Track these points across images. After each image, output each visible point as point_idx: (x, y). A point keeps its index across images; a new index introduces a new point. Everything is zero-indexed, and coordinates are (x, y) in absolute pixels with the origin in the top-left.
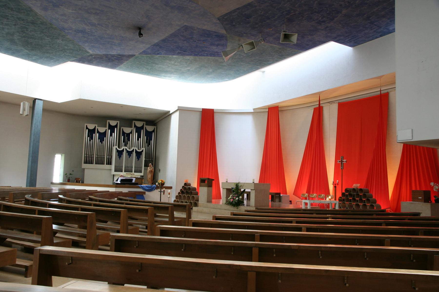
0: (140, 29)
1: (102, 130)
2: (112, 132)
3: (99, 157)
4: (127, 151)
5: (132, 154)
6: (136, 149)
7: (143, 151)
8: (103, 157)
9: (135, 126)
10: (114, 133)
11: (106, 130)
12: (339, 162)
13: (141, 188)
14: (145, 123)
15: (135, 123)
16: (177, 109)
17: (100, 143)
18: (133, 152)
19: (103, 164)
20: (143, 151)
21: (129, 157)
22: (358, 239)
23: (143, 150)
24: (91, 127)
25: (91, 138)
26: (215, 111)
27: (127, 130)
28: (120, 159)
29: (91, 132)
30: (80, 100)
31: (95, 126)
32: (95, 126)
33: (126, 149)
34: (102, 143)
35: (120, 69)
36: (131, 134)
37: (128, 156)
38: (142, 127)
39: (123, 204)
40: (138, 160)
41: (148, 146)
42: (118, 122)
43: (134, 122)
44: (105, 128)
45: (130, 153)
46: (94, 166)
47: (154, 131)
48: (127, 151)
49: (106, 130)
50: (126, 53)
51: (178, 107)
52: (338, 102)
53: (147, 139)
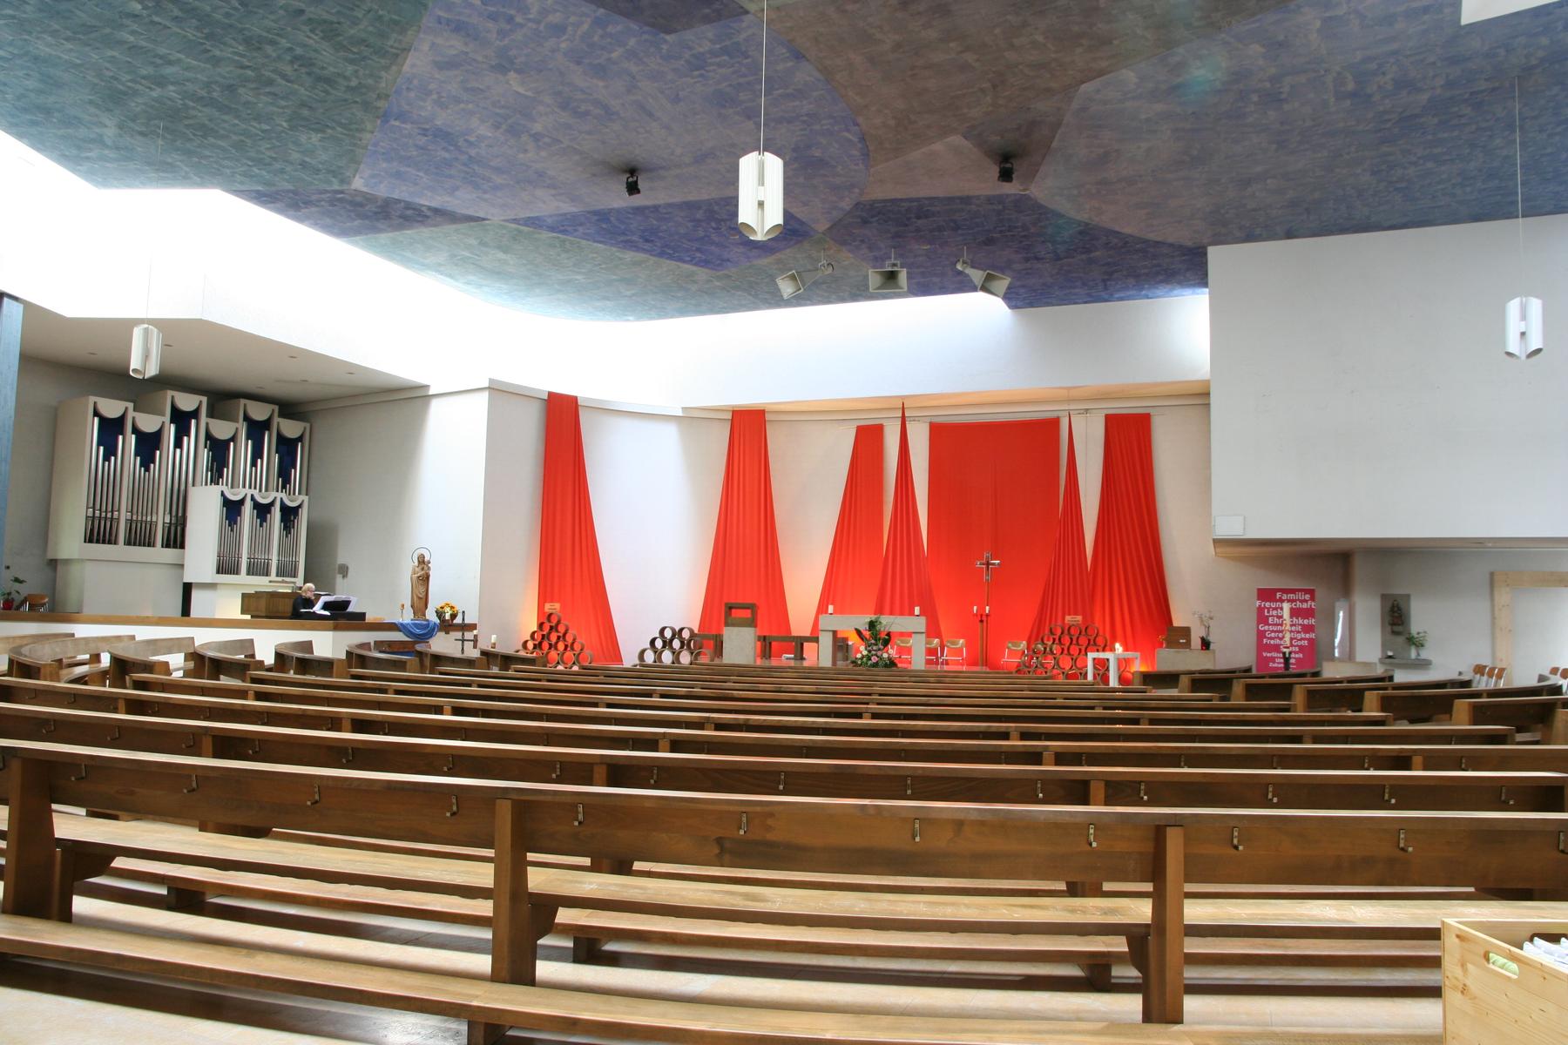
0: (632, 171)
1: (149, 423)
2: (182, 432)
3: (100, 517)
5: (269, 516)
6: (281, 499)
8: (112, 518)
9: (247, 418)
10: (189, 436)
13: (401, 631)
14: (276, 408)
15: (245, 405)
17: (143, 469)
18: (273, 508)
19: (151, 544)
21: (261, 525)
23: (303, 501)
24: (112, 408)
25: (110, 451)
27: (222, 430)
28: (232, 530)
29: (111, 429)
30: (200, 321)
32: (126, 408)
33: (252, 496)
34: (147, 470)
35: (356, 244)
36: (232, 444)
37: (259, 520)
38: (266, 425)
40: (287, 536)
41: (107, 458)
43: (243, 401)
44: (163, 419)
46: (120, 550)
47: (300, 439)
50: (428, 200)
51: (491, 380)
52: (929, 420)
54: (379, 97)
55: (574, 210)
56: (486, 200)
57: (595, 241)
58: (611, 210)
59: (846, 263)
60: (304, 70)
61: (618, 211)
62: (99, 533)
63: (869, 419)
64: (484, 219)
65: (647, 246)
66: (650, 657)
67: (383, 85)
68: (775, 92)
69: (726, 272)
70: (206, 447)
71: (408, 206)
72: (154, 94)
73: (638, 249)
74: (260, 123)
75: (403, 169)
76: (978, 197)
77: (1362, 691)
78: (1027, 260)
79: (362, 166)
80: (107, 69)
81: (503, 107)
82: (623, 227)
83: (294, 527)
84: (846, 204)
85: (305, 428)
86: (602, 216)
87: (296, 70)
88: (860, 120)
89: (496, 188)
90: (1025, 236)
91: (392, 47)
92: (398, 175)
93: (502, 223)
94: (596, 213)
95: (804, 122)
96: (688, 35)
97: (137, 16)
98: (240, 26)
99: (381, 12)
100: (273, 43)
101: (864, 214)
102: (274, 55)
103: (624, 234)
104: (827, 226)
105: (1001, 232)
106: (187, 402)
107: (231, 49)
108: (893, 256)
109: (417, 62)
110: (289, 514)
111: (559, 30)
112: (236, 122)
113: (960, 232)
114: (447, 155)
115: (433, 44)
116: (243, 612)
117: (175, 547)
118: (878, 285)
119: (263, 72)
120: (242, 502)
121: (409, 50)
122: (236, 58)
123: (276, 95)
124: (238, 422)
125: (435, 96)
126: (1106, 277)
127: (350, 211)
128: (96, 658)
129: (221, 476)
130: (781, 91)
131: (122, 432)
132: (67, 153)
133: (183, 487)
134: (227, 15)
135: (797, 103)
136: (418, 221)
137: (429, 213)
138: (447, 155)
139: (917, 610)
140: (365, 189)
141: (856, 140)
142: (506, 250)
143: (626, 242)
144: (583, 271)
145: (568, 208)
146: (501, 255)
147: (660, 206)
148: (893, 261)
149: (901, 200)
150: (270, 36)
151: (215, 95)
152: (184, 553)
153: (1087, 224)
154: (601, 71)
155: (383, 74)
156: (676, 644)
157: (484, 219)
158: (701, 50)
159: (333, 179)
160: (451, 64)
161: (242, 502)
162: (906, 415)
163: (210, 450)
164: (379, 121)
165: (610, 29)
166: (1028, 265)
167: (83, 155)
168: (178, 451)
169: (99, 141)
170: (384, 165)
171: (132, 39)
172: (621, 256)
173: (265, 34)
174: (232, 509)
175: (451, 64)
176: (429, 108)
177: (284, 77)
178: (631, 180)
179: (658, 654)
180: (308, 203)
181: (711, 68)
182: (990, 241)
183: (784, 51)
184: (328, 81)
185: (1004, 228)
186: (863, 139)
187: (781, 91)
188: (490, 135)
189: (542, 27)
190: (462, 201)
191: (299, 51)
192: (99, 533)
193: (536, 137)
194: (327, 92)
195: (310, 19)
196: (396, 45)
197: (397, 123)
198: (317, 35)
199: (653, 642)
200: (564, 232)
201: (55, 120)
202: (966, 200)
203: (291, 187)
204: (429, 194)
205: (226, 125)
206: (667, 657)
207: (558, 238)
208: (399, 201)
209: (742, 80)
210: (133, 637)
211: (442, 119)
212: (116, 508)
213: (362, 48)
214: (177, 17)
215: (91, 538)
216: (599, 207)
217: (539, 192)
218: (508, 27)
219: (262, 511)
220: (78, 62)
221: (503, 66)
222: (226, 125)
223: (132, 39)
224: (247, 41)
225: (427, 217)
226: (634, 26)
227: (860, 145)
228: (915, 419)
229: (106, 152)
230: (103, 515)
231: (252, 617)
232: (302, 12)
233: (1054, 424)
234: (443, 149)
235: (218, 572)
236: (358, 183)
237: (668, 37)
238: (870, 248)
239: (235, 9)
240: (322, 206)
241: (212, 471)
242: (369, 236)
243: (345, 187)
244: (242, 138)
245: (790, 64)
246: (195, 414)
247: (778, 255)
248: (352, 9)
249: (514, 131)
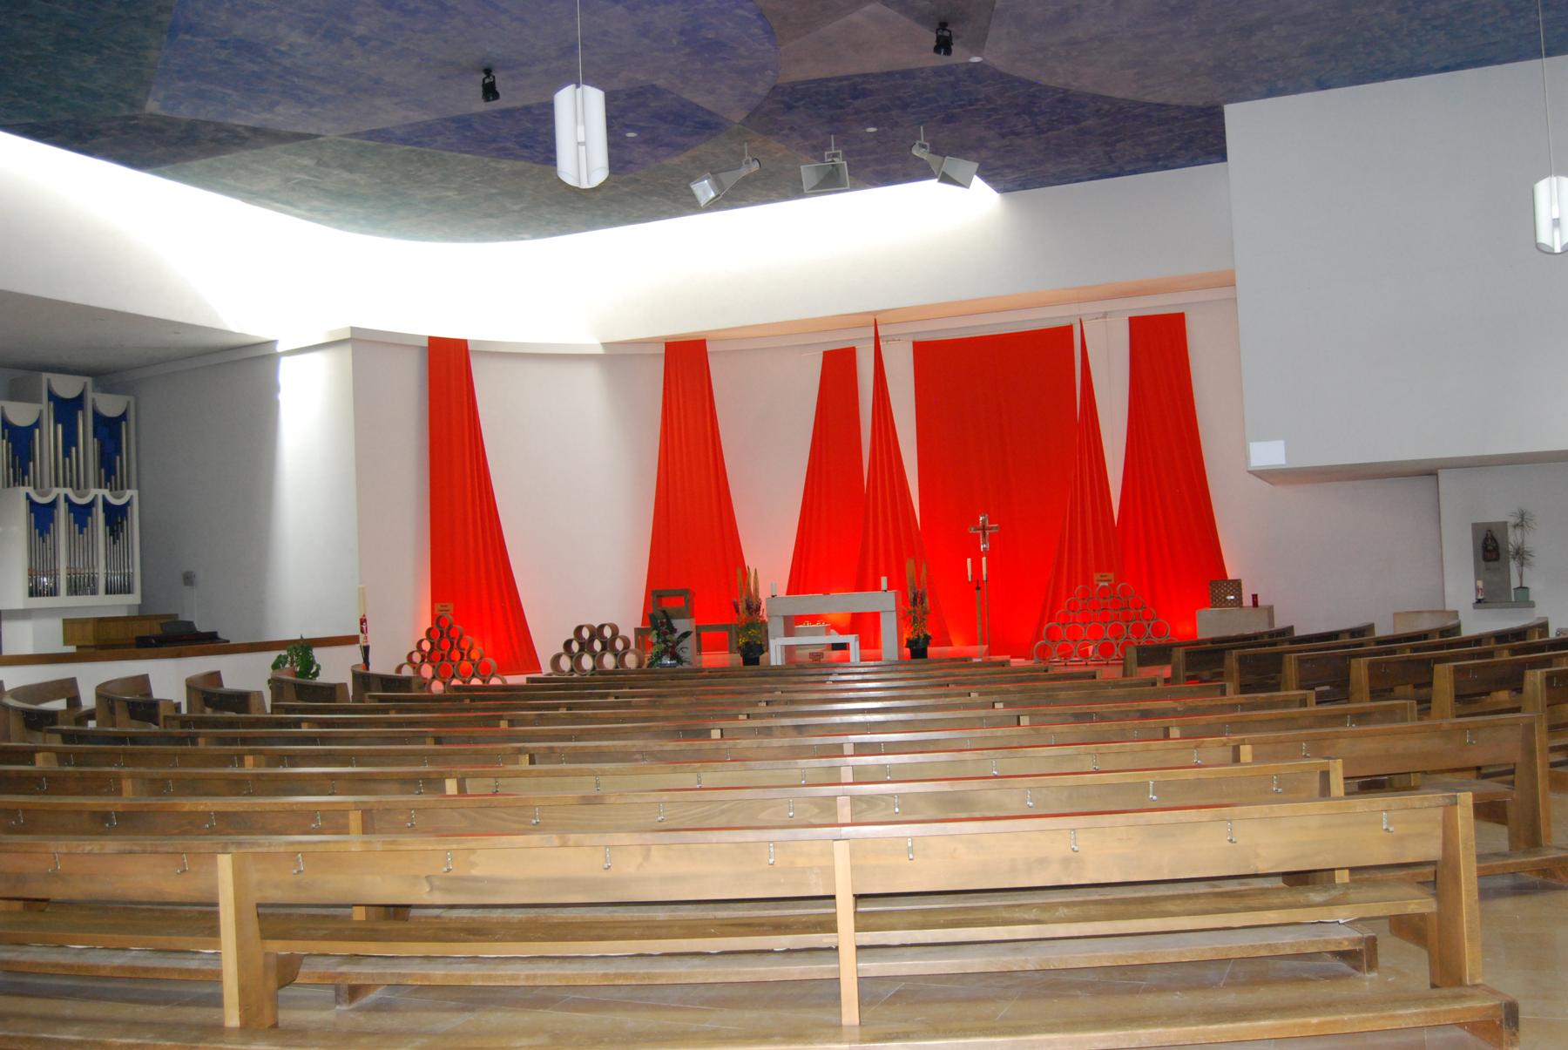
4: (72, 506)
9: (52, 396)
12: (990, 528)
21: (81, 532)
37: (77, 526)
38: (78, 402)
39: (572, 689)
40: (114, 543)
43: (45, 376)
45: (81, 514)
47: (124, 416)
48: (72, 506)
53: (102, 446)
63: (838, 341)
116: (66, 642)
139: (884, 580)
231: (78, 647)
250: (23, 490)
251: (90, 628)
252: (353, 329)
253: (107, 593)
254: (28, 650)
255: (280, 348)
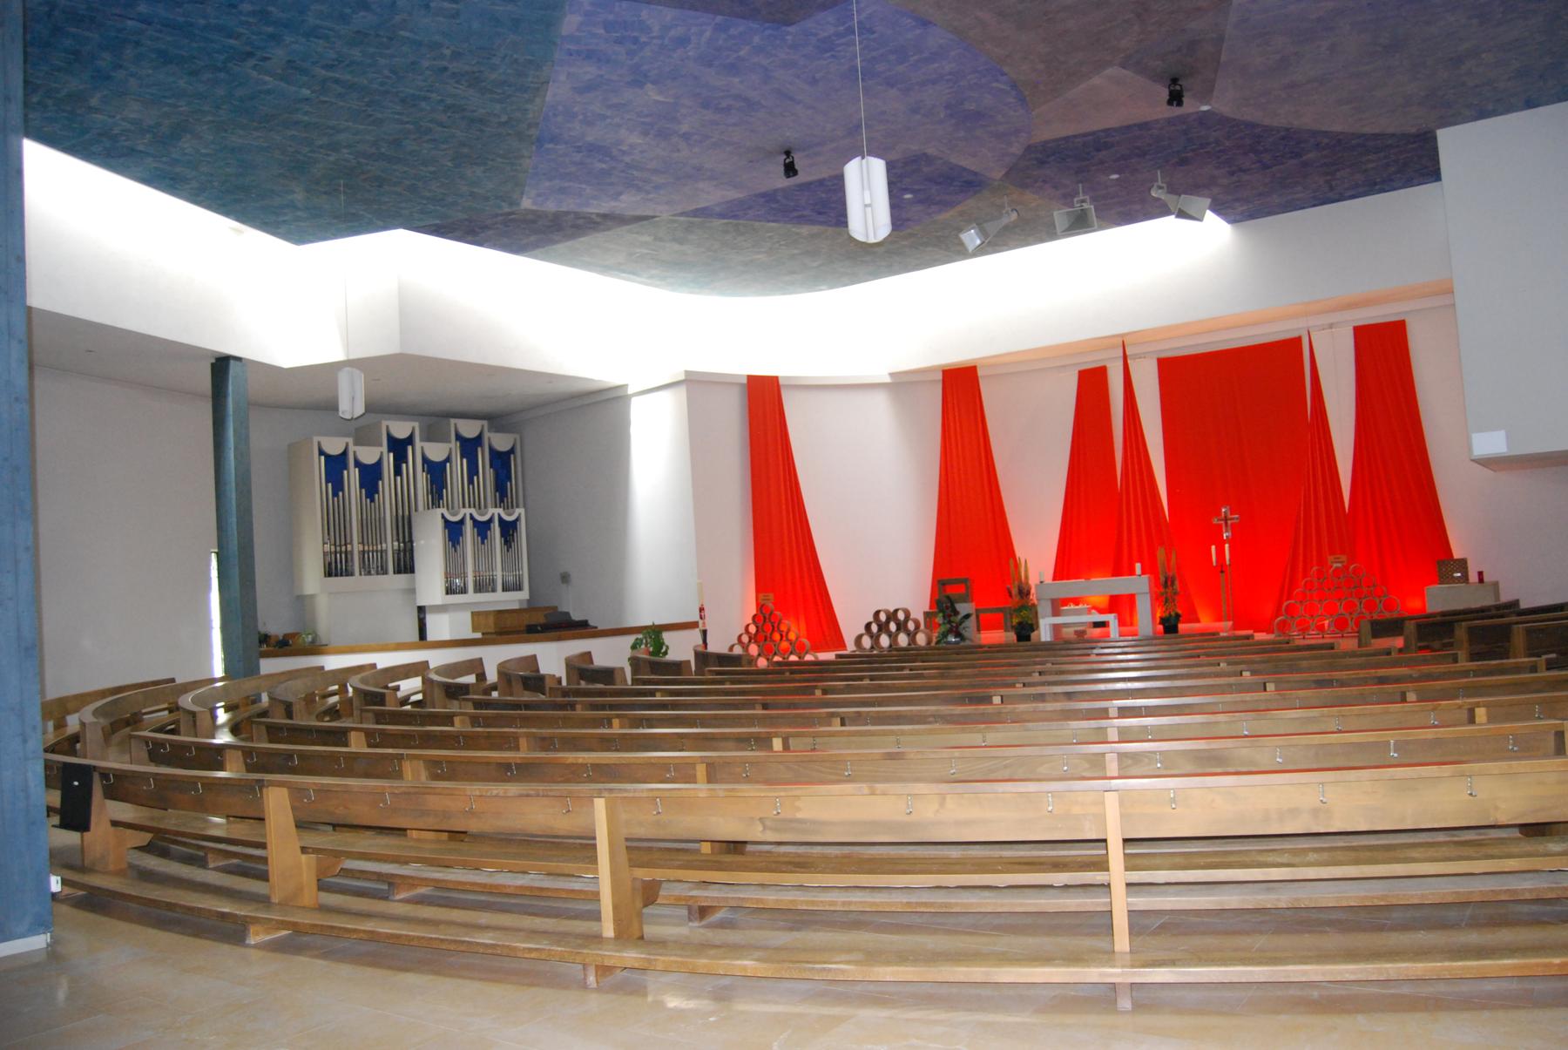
1: (369, 455)
2: (400, 458)
4: (476, 523)
7: (518, 519)
9: (459, 437)
10: (407, 463)
11: (382, 453)
16: (682, 377)
18: (492, 525)
20: (518, 519)
21: (483, 543)
22: (1145, 707)
24: (334, 447)
26: (781, 382)
29: (336, 465)
30: (401, 354)
31: (448, 450)
32: (347, 444)
33: (471, 515)
34: (372, 500)
37: (479, 538)
38: (478, 440)
40: (508, 551)
41: (335, 494)
42: (416, 425)
43: (453, 421)
44: (380, 449)
47: (512, 451)
48: (476, 523)
49: (382, 453)
54: (530, 126)
55: (741, 196)
56: (651, 200)
57: (769, 221)
58: (776, 191)
59: (1033, 205)
60: (457, 116)
61: (783, 190)
62: (335, 568)
63: (1090, 362)
64: (653, 217)
65: (822, 218)
66: (867, 642)
67: (531, 116)
68: (912, 59)
69: (909, 231)
70: (423, 471)
71: (577, 215)
72: (332, 159)
73: (813, 222)
74: (426, 166)
75: (567, 184)
76: (1157, 121)
77: (1451, 623)
78: (1232, 173)
79: (527, 189)
80: (290, 146)
81: (647, 116)
82: (792, 204)
83: (514, 541)
84: (1017, 149)
85: (515, 440)
86: (769, 197)
87: (449, 117)
88: (1006, 69)
89: (657, 188)
90: (1220, 151)
91: (532, 82)
92: (562, 191)
93: (670, 218)
94: (764, 195)
95: (948, 81)
96: (809, 24)
97: (307, 99)
98: (394, 90)
99: (515, 56)
100: (425, 99)
101: (1039, 155)
102: (428, 108)
103: (795, 210)
104: (1003, 172)
105: (1193, 150)
106: (401, 430)
107: (390, 111)
108: (1081, 191)
109: (559, 90)
110: (508, 529)
111: (683, 41)
112: (406, 169)
113: (1148, 157)
114: (604, 166)
115: (569, 74)
116: (475, 629)
117: (405, 572)
118: (1067, 226)
119: (422, 124)
120: (462, 522)
121: (548, 83)
122: (396, 116)
123: (434, 140)
124: (450, 442)
125: (581, 117)
126: (1329, 178)
127: (524, 228)
128: (343, 689)
129: (441, 497)
130: (915, 58)
131: (345, 467)
132: (267, 220)
133: (407, 513)
134: (382, 84)
135: (936, 65)
136: (591, 228)
137: (599, 220)
138: (604, 166)
139: (1138, 566)
140: (534, 208)
141: (1009, 88)
142: (681, 241)
143: (799, 217)
144: (763, 250)
145: (733, 195)
146: (676, 247)
147: (824, 179)
148: (1082, 198)
149: (1075, 136)
150: (422, 93)
151: (383, 150)
152: (413, 581)
153: (1287, 130)
154: (733, 69)
155: (529, 106)
156: (893, 627)
157: (653, 217)
158: (826, 34)
159: (503, 204)
160: (589, 87)
161: (462, 522)
162: (1128, 353)
163: (427, 474)
164: (534, 148)
165: (733, 31)
166: (1235, 178)
167: (281, 219)
168: (399, 478)
169: (292, 206)
170: (547, 184)
171: (306, 118)
172: (798, 231)
173: (418, 93)
174: (453, 531)
175: (589, 87)
176: (578, 128)
177: (441, 125)
178: (787, 161)
179: (875, 639)
180: (485, 228)
181: (839, 48)
182: (1183, 162)
183: (909, 21)
184: (481, 121)
185: (1194, 147)
186: (1014, 86)
187: (915, 58)
188: (640, 141)
189: (666, 41)
190: (627, 203)
191: (449, 101)
192: (335, 568)
193: (686, 137)
194: (481, 131)
195: (454, 73)
196: (535, 80)
197: (551, 146)
198: (462, 85)
199: (868, 626)
200: (735, 217)
201: (253, 196)
202: (1144, 126)
203: (466, 217)
204: (595, 202)
205: (397, 173)
206: (885, 641)
207: (731, 223)
208: (567, 213)
209: (874, 54)
210: (374, 666)
211: (592, 135)
212: (348, 541)
213: (506, 88)
214: (340, 94)
215: (330, 571)
216: (763, 189)
217: (701, 185)
218: (635, 47)
219: (482, 528)
220: (265, 145)
221: (639, 79)
222: (397, 173)
223: (306, 118)
224: (403, 101)
225: (598, 223)
226: (755, 26)
227: (1014, 93)
228: (1137, 356)
229: (299, 213)
230: (338, 549)
231: (483, 634)
232: (446, 69)
233: (1296, 342)
234: (600, 161)
235: (447, 593)
236: (526, 203)
237: (790, 29)
238: (1055, 187)
239: (388, 77)
240: (497, 228)
241: (432, 493)
242: (546, 248)
243: (514, 209)
244: (414, 182)
245: (918, 32)
246: (410, 440)
247: (959, 208)
248: (489, 58)
249: (663, 135)
250: (439, 511)
251: (491, 619)
252: (686, 372)
253: (503, 590)
254: (446, 637)
255: (630, 391)
